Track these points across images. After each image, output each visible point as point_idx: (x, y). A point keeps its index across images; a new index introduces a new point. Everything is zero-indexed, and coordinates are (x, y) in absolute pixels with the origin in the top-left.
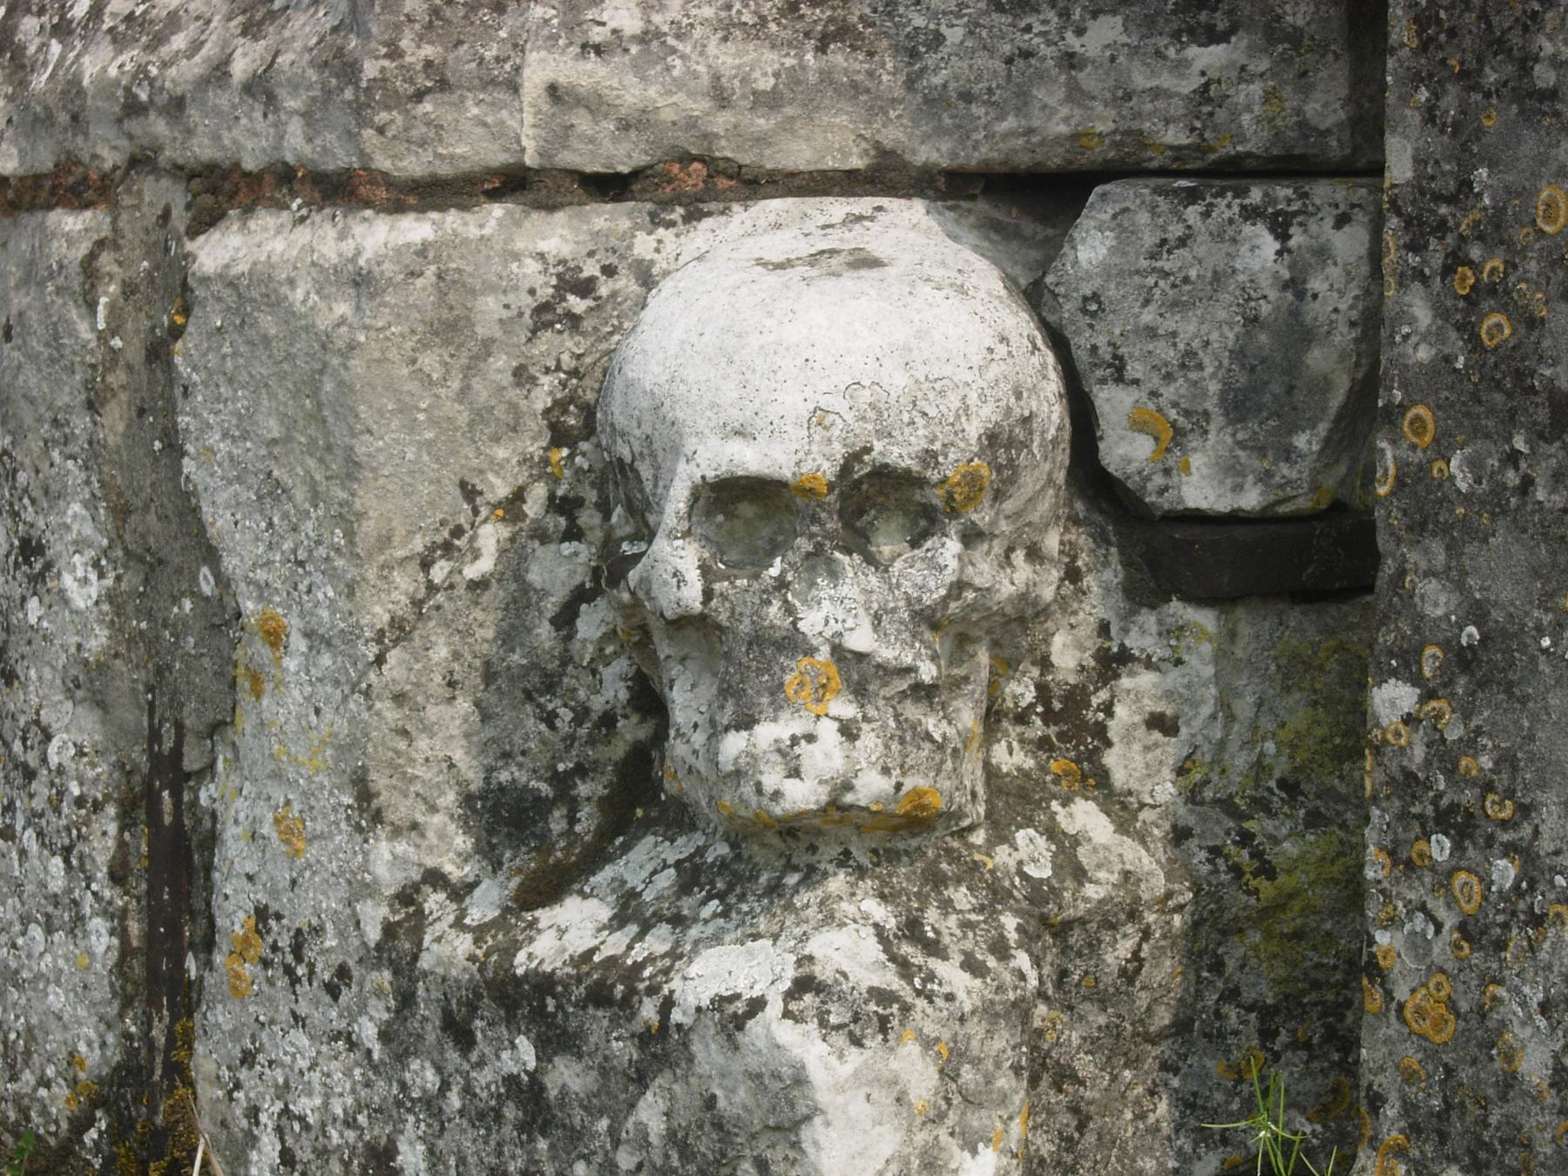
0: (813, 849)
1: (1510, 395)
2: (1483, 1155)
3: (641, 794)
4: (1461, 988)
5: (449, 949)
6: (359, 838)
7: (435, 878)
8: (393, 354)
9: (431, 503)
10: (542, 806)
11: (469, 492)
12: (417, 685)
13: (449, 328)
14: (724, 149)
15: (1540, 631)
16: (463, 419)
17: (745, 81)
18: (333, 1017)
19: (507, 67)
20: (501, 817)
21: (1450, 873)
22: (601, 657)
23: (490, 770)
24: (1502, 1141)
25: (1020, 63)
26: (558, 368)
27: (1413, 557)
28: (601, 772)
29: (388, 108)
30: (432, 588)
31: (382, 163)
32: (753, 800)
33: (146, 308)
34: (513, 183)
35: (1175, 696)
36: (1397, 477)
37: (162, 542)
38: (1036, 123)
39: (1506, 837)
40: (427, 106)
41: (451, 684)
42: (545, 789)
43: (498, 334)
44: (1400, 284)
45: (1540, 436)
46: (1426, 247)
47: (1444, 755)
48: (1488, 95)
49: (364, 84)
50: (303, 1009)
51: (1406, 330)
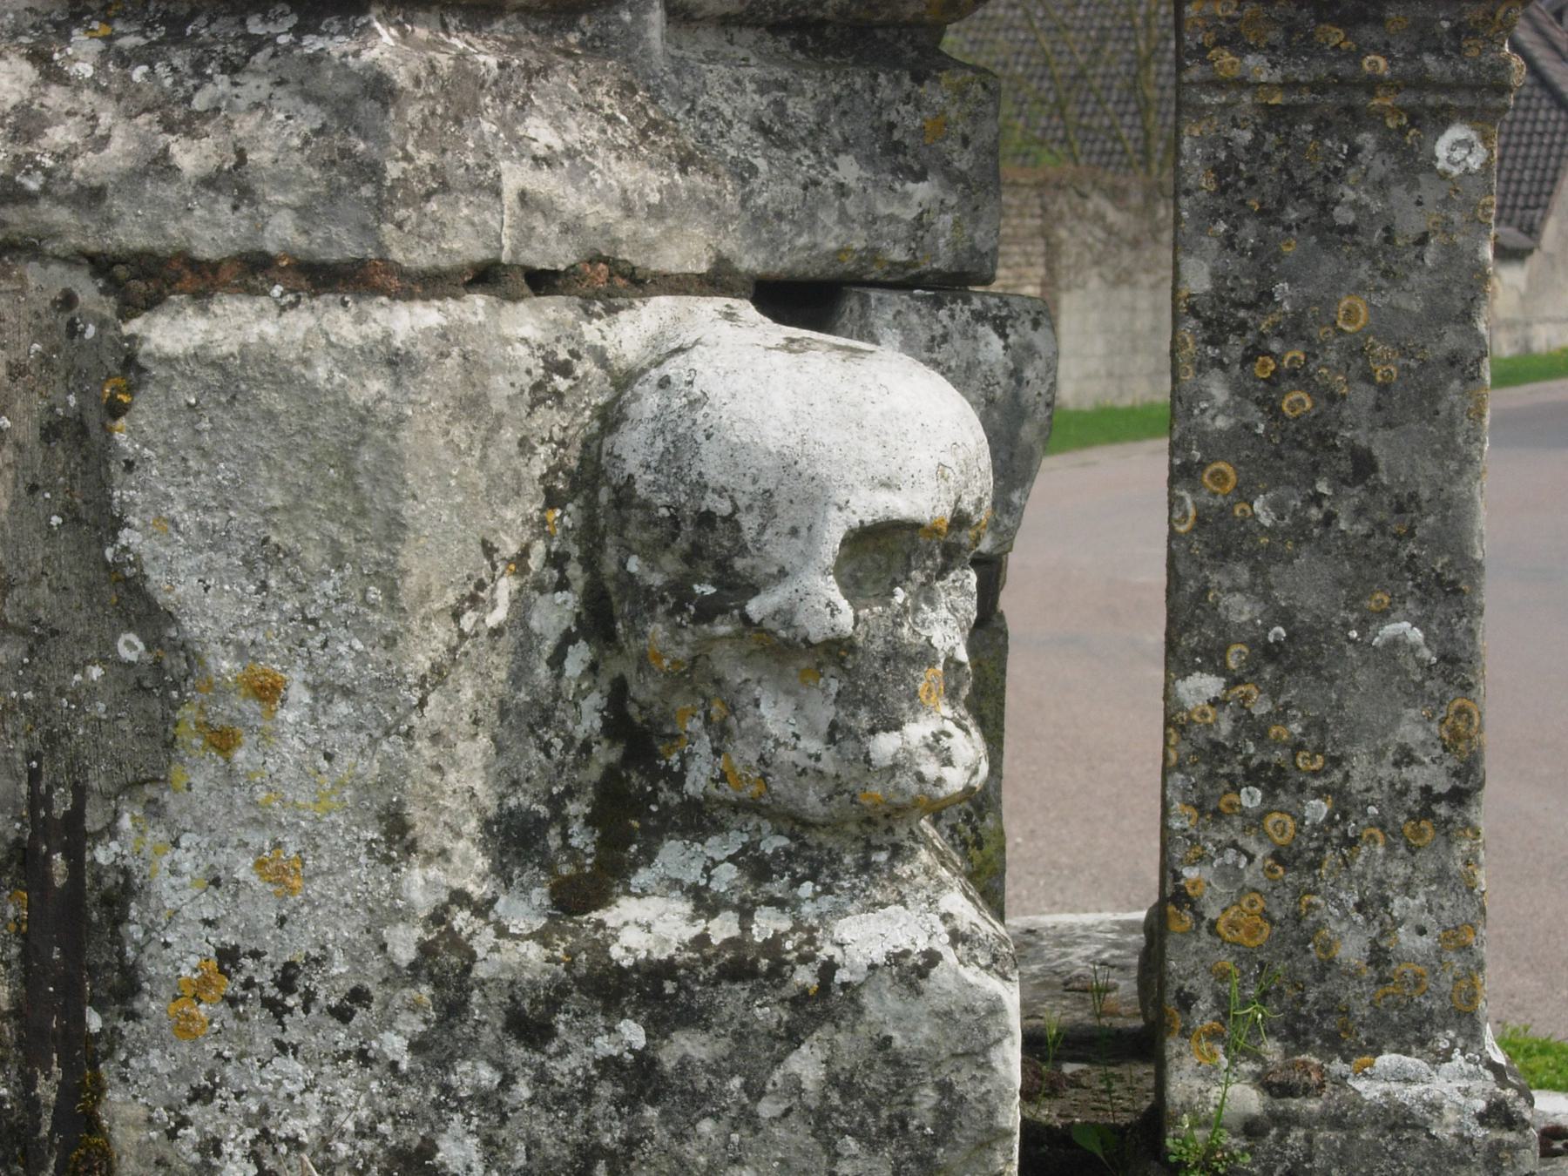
0: (890, 830)
1: (1312, 452)
2: (1300, 1026)
4: (1275, 902)
6: (386, 869)
7: (460, 898)
8: (434, 427)
9: (460, 560)
10: (542, 825)
11: (488, 550)
12: (450, 724)
13: (472, 404)
14: (625, 254)
15: (1346, 626)
16: (482, 485)
17: (641, 195)
18: (342, 1037)
19: (490, 173)
21: (1262, 816)
22: (581, 694)
23: (502, 797)
24: (1319, 1013)
25: (812, 189)
26: (551, 439)
27: (1215, 578)
29: (407, 205)
30: (463, 636)
31: (397, 255)
32: (914, 788)
33: (41, 388)
34: (484, 276)
36: (1197, 518)
38: (819, 239)
39: (1317, 783)
40: (433, 206)
41: (476, 722)
42: (543, 811)
43: (506, 410)
44: (1199, 370)
45: (1340, 481)
46: (1226, 341)
47: (1250, 726)
48: (1288, 228)
49: (388, 183)
50: (293, 1035)
51: (1204, 405)
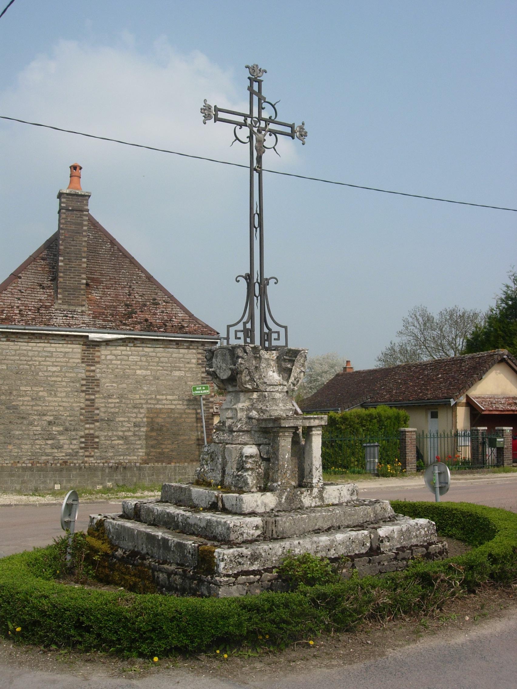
3: (243, 468)
5: (235, 474)
20: (237, 469)
28: (241, 467)
35: (263, 465)
37: (224, 458)
